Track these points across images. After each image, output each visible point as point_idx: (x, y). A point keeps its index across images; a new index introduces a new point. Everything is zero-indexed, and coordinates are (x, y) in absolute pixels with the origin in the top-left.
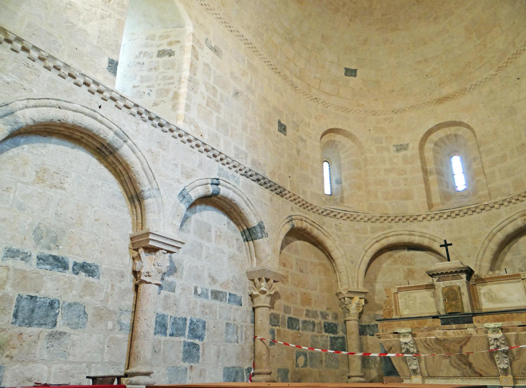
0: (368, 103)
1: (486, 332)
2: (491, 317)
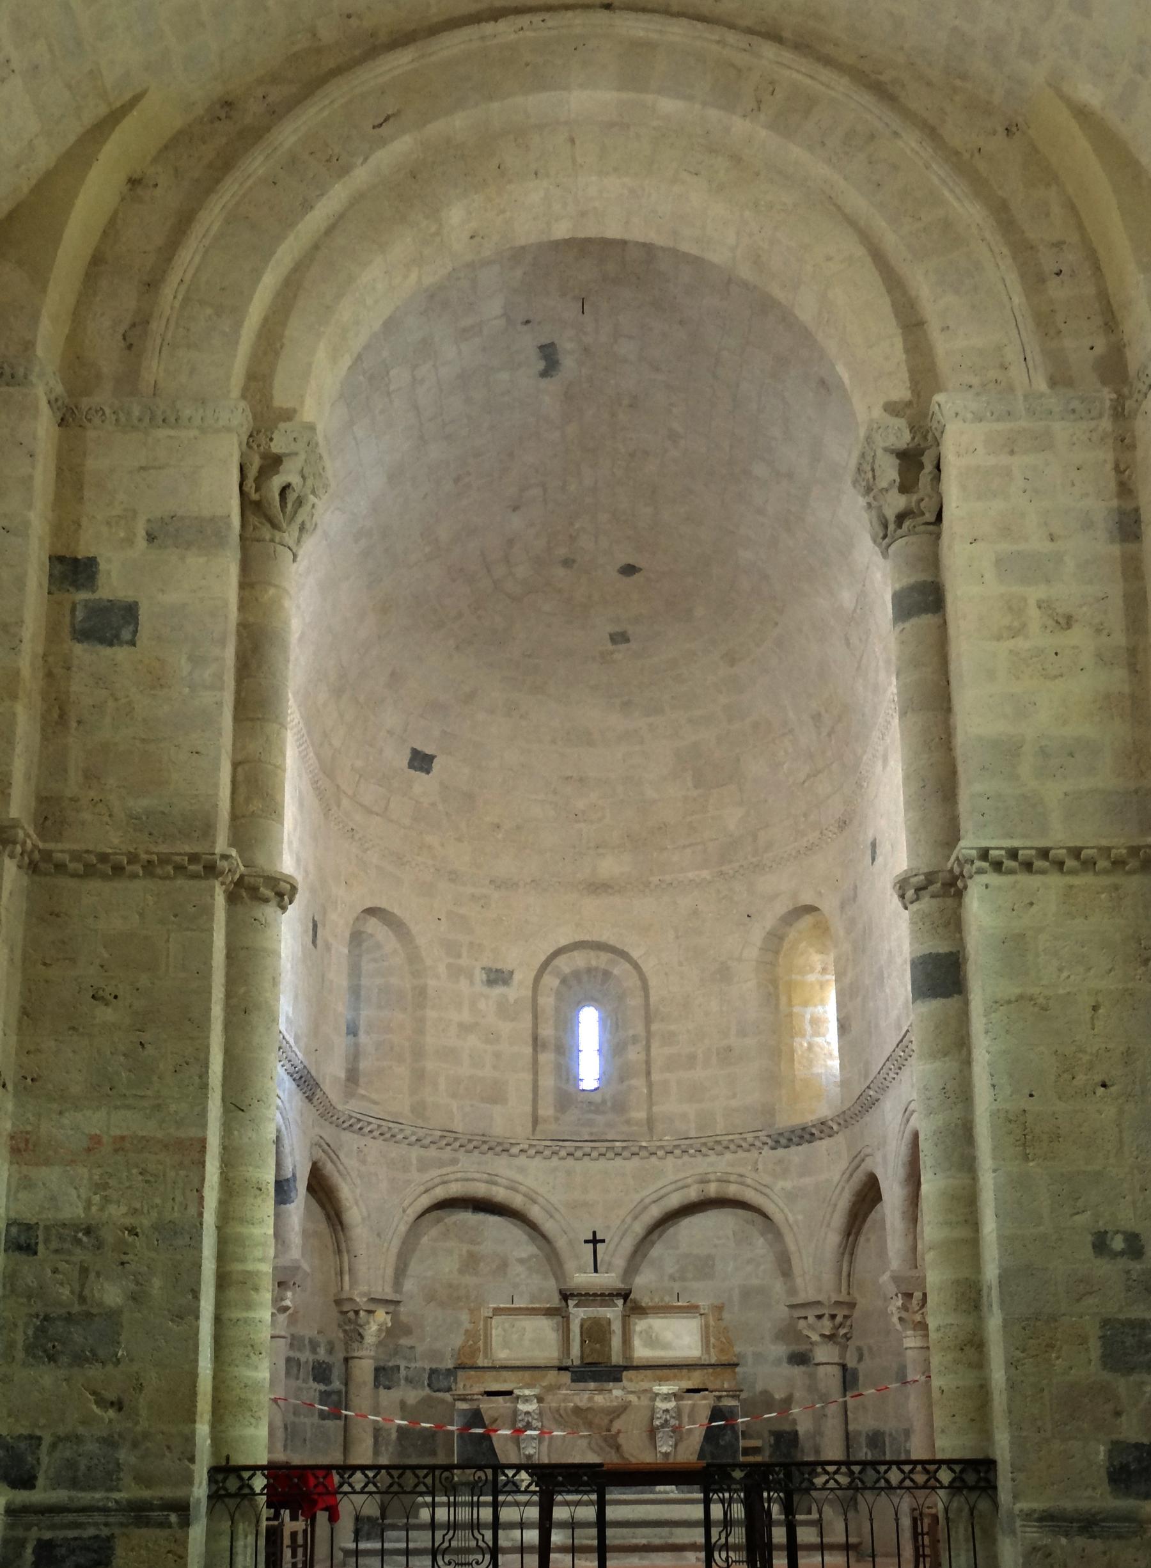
0: (443, 845)
1: (653, 1399)
2: (649, 1372)
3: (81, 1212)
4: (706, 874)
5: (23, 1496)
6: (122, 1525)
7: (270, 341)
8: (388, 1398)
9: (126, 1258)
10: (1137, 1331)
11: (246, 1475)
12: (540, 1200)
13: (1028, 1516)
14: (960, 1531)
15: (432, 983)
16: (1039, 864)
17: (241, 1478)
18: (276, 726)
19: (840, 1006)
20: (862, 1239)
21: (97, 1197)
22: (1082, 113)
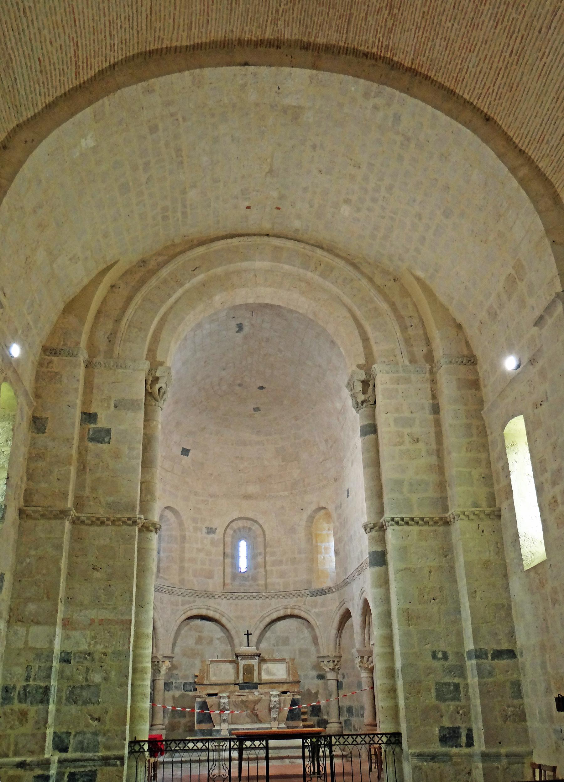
1: (270, 697)
2: (268, 685)
3: (87, 648)
4: (286, 493)
5: (64, 755)
6: (100, 766)
7: (156, 339)
8: (169, 694)
9: (103, 664)
10: (447, 686)
11: (142, 744)
12: (226, 615)
13: (413, 755)
14: (390, 759)
15: (187, 534)
16: (410, 523)
17: (140, 745)
18: (155, 469)
19: (335, 545)
20: (344, 632)
21: (93, 642)
22: (418, 279)
